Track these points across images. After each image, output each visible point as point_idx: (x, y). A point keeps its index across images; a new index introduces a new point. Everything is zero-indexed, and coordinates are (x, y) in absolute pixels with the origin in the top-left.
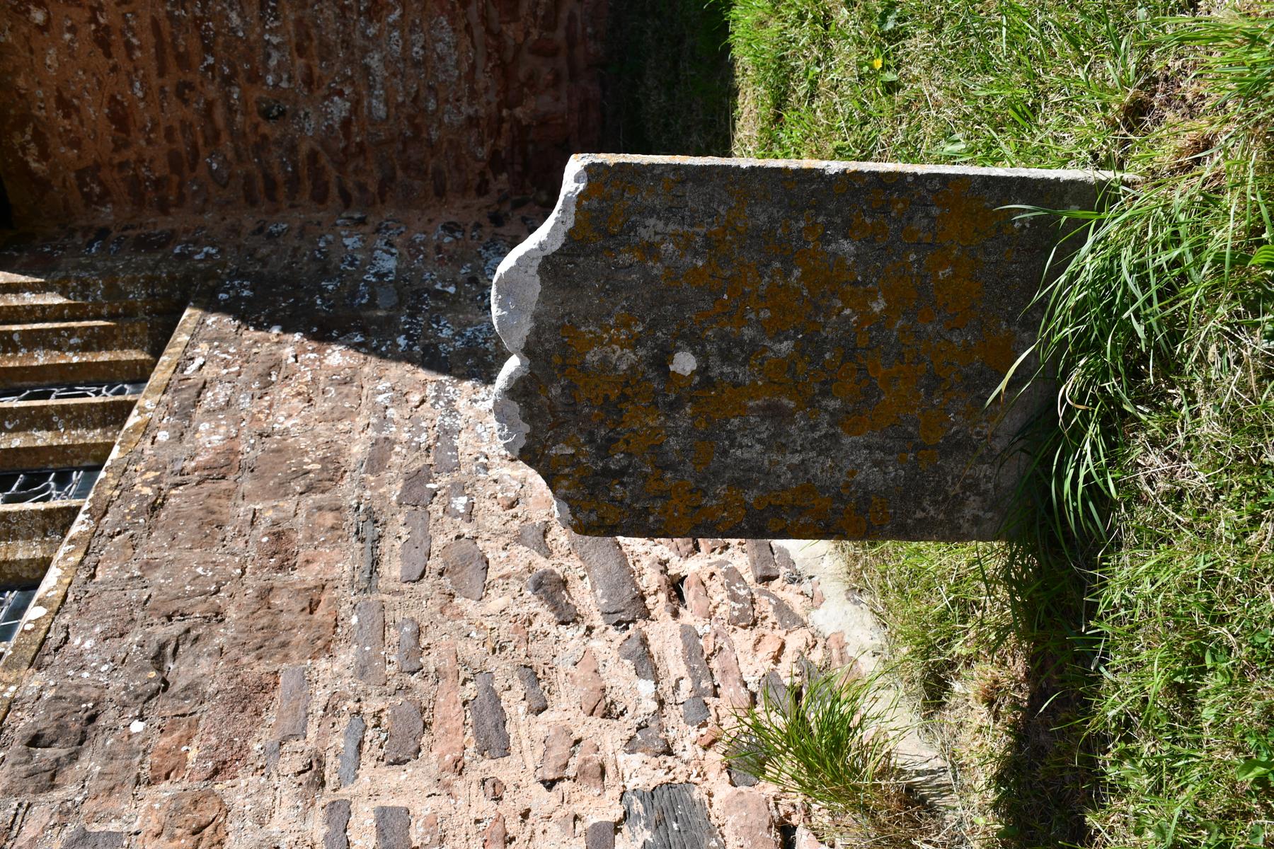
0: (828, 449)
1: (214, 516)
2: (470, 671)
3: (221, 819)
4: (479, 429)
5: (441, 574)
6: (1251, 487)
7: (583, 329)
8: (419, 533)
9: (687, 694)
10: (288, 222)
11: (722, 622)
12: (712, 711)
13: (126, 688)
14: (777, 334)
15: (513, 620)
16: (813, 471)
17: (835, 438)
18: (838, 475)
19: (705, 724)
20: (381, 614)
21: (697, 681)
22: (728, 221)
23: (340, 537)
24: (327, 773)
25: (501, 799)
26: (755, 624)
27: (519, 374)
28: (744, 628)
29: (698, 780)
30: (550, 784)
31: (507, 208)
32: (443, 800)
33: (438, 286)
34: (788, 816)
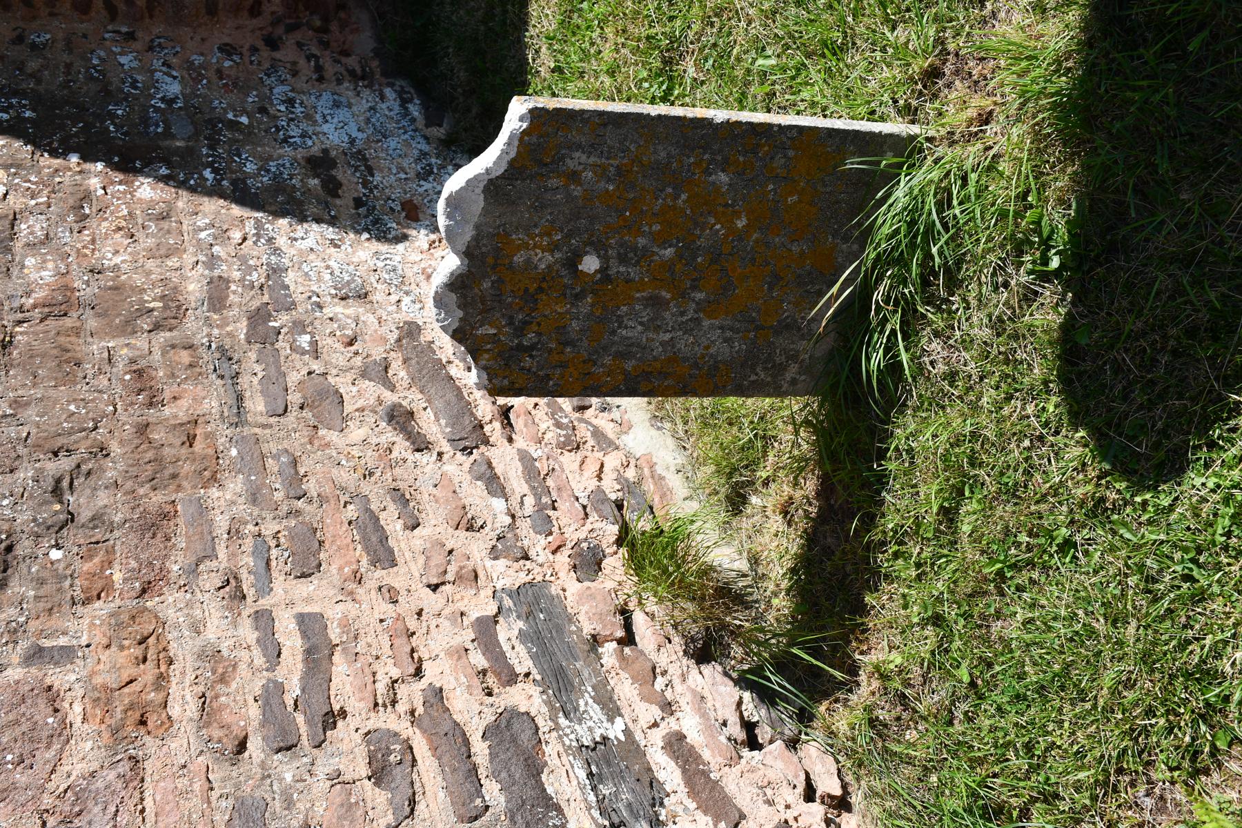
0: (692, 330)
1: (69, 354)
2: (347, 496)
3: (160, 630)
4: (305, 268)
5: (302, 408)
6: (1007, 376)
7: (514, 237)
8: (273, 370)
9: (531, 509)
10: (49, 32)
11: (550, 446)
12: (555, 522)
13: (34, 520)
14: (664, 243)
15: (376, 448)
16: (679, 346)
17: (697, 321)
18: (697, 349)
19: (551, 533)
20: (257, 446)
21: (538, 498)
22: (636, 156)
23: (200, 374)
24: (245, 587)
25: (397, 601)
26: (578, 448)
27: (459, 272)
28: (570, 451)
29: (552, 579)
30: (434, 588)
31: (280, 30)
32: (350, 605)
33: (230, 116)
34: (626, 604)
